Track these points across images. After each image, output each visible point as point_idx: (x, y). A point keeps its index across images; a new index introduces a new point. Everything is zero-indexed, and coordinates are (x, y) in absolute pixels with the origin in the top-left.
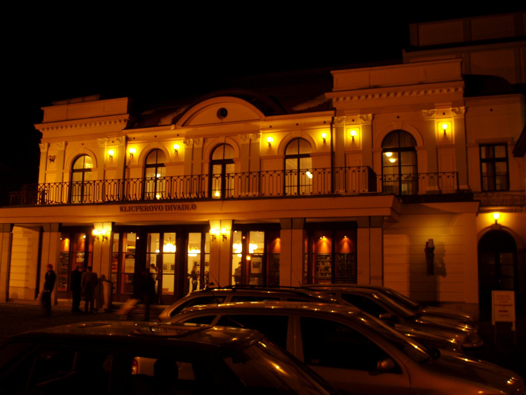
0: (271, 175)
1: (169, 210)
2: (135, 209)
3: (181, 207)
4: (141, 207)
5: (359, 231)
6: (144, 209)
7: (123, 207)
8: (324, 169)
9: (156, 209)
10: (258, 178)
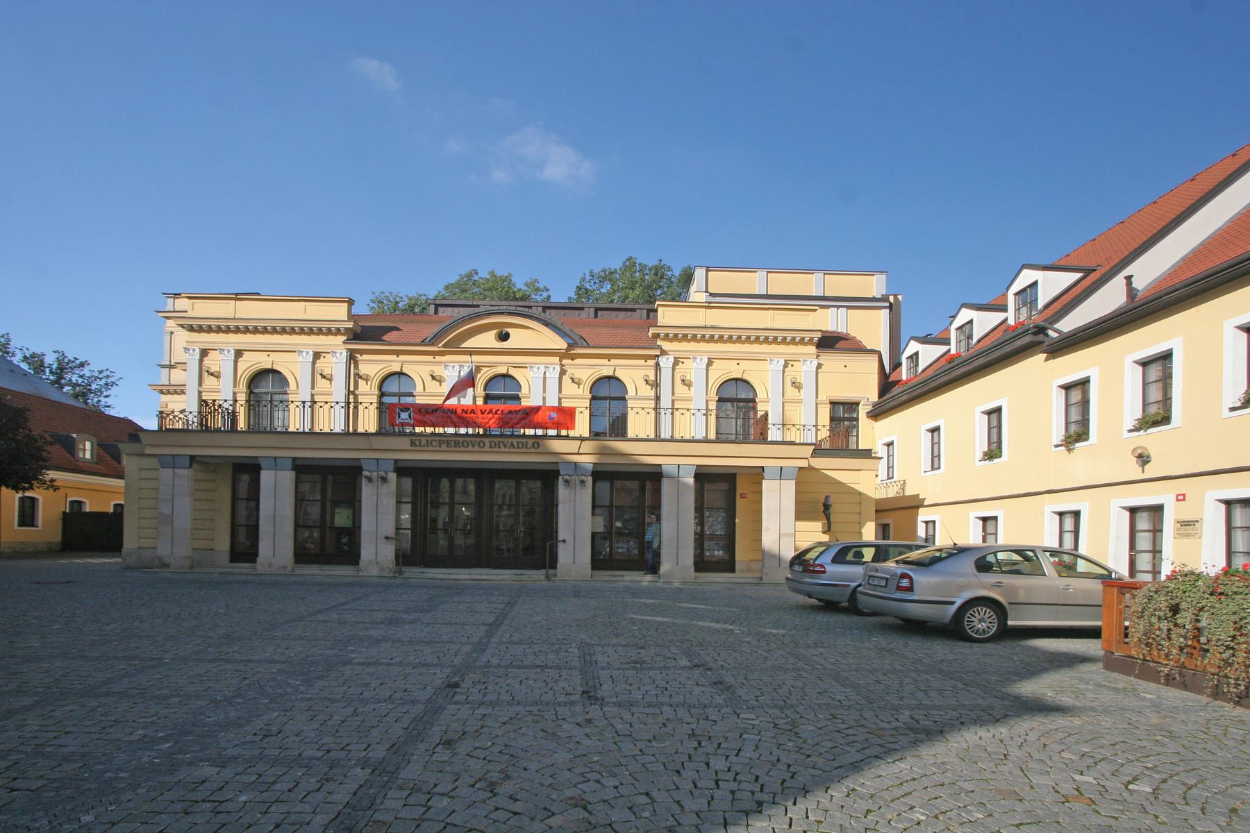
0: (366, 408)
1: (495, 446)
2: (438, 443)
3: (515, 444)
4: (447, 441)
5: (765, 484)
6: (452, 444)
7: (415, 440)
8: (304, 403)
9: (473, 446)
10: (302, 408)
